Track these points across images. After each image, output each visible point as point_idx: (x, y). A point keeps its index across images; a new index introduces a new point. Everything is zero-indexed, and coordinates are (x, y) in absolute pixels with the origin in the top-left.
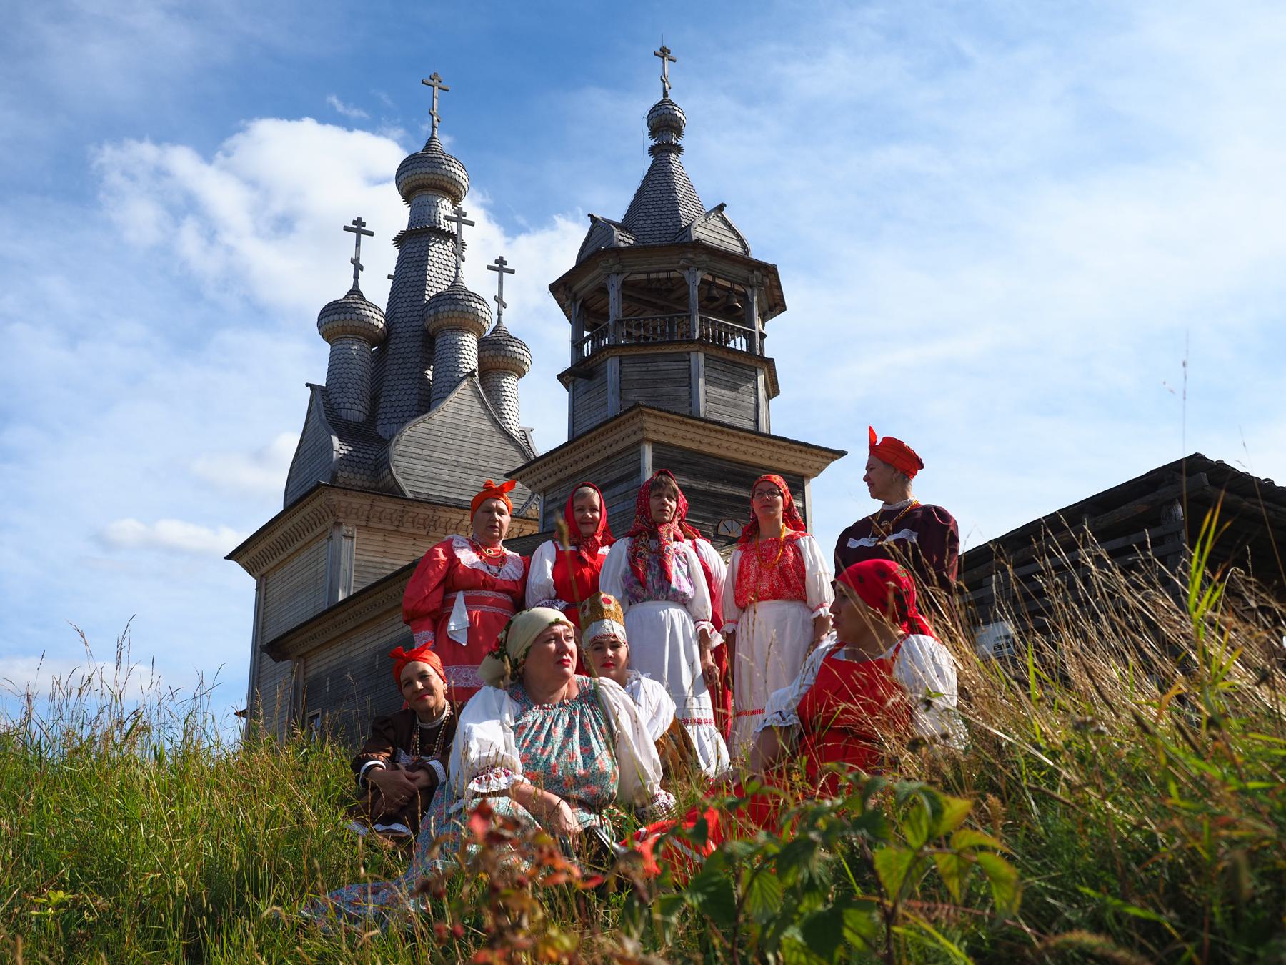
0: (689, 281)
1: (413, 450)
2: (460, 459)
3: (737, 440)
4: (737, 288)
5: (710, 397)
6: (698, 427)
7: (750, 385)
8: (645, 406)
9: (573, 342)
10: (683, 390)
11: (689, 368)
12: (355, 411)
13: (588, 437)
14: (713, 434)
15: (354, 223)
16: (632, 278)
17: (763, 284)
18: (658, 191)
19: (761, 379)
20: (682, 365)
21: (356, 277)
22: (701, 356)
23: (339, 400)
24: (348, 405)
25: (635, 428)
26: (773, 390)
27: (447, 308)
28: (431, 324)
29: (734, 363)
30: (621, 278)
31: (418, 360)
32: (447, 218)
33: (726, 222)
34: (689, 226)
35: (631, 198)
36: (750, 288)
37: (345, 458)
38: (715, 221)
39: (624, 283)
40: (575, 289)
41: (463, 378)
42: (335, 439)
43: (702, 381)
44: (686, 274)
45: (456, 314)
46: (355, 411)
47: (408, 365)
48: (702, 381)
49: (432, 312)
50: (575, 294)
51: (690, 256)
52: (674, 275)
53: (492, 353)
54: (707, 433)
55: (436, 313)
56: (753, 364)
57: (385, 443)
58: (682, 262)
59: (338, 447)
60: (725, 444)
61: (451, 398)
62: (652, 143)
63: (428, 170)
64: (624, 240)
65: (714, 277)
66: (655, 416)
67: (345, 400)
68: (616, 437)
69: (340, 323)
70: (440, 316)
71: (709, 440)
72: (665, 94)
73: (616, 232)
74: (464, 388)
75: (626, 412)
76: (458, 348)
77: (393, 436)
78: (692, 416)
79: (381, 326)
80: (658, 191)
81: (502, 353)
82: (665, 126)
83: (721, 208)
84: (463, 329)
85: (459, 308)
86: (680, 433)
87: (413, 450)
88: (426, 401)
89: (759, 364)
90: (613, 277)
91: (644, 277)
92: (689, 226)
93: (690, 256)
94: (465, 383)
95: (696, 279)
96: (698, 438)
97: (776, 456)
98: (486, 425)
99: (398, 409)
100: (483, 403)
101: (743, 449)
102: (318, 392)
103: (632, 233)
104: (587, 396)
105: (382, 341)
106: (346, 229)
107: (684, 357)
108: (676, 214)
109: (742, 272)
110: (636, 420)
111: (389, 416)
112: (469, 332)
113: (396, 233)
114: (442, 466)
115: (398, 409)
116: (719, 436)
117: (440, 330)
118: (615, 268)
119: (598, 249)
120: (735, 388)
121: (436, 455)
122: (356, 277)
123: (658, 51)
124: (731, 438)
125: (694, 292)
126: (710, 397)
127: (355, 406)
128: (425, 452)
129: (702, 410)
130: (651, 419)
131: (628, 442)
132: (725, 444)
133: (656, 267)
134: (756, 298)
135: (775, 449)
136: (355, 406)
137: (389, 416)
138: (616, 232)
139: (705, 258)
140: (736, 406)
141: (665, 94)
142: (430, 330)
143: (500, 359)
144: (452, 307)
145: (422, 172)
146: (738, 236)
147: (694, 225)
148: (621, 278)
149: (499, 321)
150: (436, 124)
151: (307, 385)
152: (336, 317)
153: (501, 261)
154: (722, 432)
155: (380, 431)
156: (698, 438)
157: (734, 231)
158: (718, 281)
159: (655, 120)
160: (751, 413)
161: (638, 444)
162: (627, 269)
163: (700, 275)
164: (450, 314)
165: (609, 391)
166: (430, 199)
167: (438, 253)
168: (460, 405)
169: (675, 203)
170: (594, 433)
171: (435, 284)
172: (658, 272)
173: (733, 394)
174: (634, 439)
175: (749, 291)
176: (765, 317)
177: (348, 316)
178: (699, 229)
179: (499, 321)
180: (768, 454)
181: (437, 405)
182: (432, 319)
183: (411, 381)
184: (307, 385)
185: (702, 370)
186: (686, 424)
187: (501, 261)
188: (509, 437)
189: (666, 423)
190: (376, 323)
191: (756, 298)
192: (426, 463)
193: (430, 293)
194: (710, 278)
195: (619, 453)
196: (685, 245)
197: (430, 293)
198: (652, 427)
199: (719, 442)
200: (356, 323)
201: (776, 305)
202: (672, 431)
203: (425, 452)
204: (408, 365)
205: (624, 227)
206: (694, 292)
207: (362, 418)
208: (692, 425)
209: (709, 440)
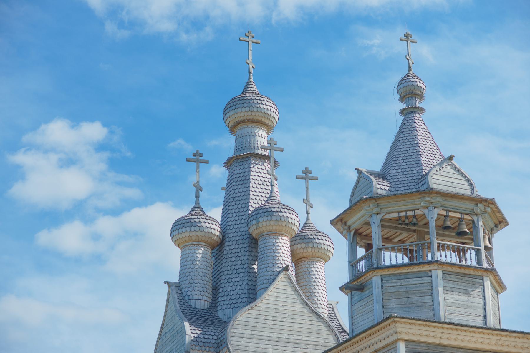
0: (429, 217)
1: (244, 332)
2: (280, 336)
3: (468, 334)
4: (466, 217)
5: (450, 302)
6: (438, 327)
7: (479, 290)
8: (397, 317)
9: (350, 262)
10: (428, 299)
11: (431, 282)
12: (201, 301)
13: (361, 336)
14: (450, 331)
15: (194, 155)
16: (388, 216)
17: (486, 212)
18: (405, 144)
19: (487, 284)
20: (426, 280)
21: (197, 197)
22: (440, 272)
23: (189, 293)
24: (196, 297)
25: (392, 331)
26: (500, 287)
27: (265, 219)
28: (254, 231)
29: (466, 275)
30: (380, 217)
31: (246, 258)
32: (262, 148)
33: (455, 169)
34: (427, 174)
35: (387, 150)
36: (470, 220)
37: (196, 341)
38: (447, 169)
39: (382, 220)
40: (349, 223)
41: (279, 273)
42: (187, 324)
43: (441, 290)
44: (426, 211)
45: (272, 223)
46: (201, 301)
47: (239, 263)
48: (441, 290)
49: (254, 222)
50: (349, 227)
51: (428, 199)
52: (417, 212)
53: (303, 245)
54: (445, 331)
55: (258, 222)
56: (480, 273)
57: (224, 324)
58: (422, 204)
59: (190, 332)
60: (460, 338)
61: (271, 288)
62: (403, 106)
63: (247, 109)
64: (381, 187)
65: (448, 211)
66: (405, 323)
67: (193, 293)
68: (380, 337)
69: (187, 234)
70: (260, 225)
71: (447, 336)
72: (410, 69)
73: (375, 181)
74: (281, 280)
75: (384, 321)
76: (274, 248)
77: (230, 318)
78: (435, 321)
79: (218, 233)
80: (405, 144)
81: (311, 245)
82: (410, 94)
83: (451, 158)
84: (277, 234)
85: (274, 218)
86: (425, 333)
87: (244, 332)
88: (252, 295)
89: (485, 274)
90: (374, 217)
91: (396, 215)
92: (427, 174)
93: (428, 199)
94: (281, 276)
95: (433, 215)
96: (439, 335)
97: (500, 343)
98: (299, 308)
99: (233, 297)
100: (296, 291)
101: (474, 339)
102: (173, 288)
103: (387, 180)
104: (360, 303)
105: (218, 247)
106: (188, 160)
107: (427, 275)
108: (419, 163)
109: (468, 206)
110: (392, 326)
111: (226, 302)
112: (283, 235)
113: (226, 159)
114: (267, 342)
115: (233, 297)
116: (455, 332)
117: (262, 235)
118: (375, 210)
119: (362, 197)
120: (467, 293)
121: (262, 334)
122: (197, 197)
123: (403, 37)
124: (464, 333)
125: (433, 225)
126: (450, 302)
127: (201, 297)
128: (253, 333)
129: (442, 313)
130: (403, 325)
131: (388, 341)
132: (460, 338)
133: (404, 208)
134: (481, 223)
135: (498, 338)
136: (201, 297)
137: (226, 302)
138: (375, 181)
139: (439, 199)
140: (468, 307)
141: (410, 69)
142: (254, 235)
143: (309, 250)
144: (269, 218)
145: (242, 113)
146: (466, 177)
147: (431, 174)
148: (380, 217)
149: (308, 219)
150: (251, 70)
151: (165, 283)
152: (184, 229)
153: (307, 172)
154: (456, 329)
155: (220, 314)
156: (439, 335)
157: (462, 174)
158: (451, 214)
159: (402, 90)
160: (481, 312)
161: (395, 342)
162: (383, 210)
163: (436, 211)
164: (268, 223)
165: (375, 301)
166: (250, 130)
167: (258, 172)
168: (279, 295)
169: (418, 154)
170: (364, 335)
171: (256, 202)
172: (406, 211)
173: (464, 298)
174: (392, 339)
175: (475, 218)
176: (491, 232)
177: (193, 229)
178: (435, 177)
179: (308, 219)
180: (494, 342)
181: (261, 295)
182: (255, 227)
183: (241, 275)
184: (165, 283)
185: (441, 282)
186: (429, 326)
187: (307, 172)
188: (318, 315)
189: (414, 327)
190: (214, 232)
191: (481, 223)
192: (255, 341)
193: (253, 205)
194: (444, 213)
195: (383, 348)
196: (423, 192)
197: (253, 205)
198: (404, 330)
199: (455, 337)
200: (199, 234)
201: (500, 222)
202: (419, 332)
203: (253, 333)
204: (239, 263)
205: (382, 176)
206: (433, 225)
207: (206, 305)
208: (434, 327)
209: (447, 336)
